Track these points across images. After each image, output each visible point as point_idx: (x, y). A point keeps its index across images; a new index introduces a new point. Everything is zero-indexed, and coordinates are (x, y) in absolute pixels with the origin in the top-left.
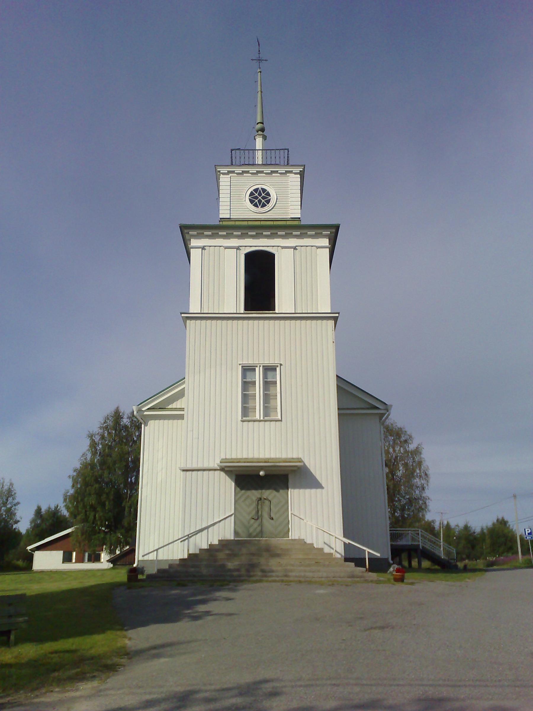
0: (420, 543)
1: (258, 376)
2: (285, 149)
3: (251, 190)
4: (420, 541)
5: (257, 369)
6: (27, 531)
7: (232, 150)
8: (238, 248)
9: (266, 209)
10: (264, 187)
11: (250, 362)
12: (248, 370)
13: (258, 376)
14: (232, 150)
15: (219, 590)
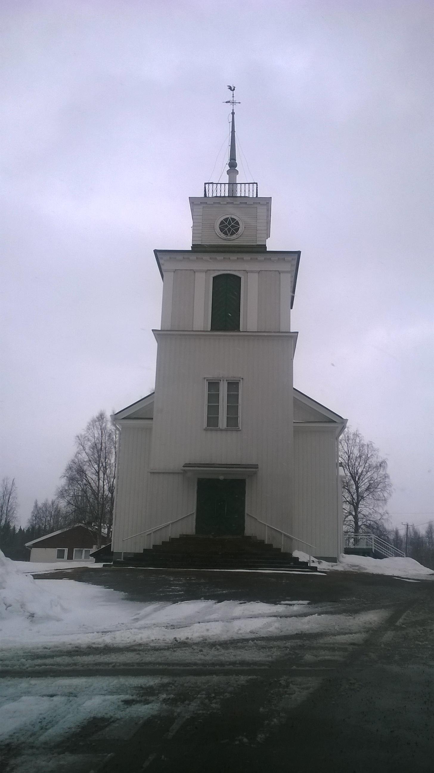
0: (373, 548)
1: (223, 422)
2: (254, 183)
3: (222, 219)
4: (373, 545)
5: (221, 383)
6: (39, 512)
7: (205, 184)
8: (207, 271)
9: (234, 236)
10: (233, 217)
11: (213, 374)
12: (213, 385)
13: (223, 422)
14: (205, 184)
15: (149, 721)
